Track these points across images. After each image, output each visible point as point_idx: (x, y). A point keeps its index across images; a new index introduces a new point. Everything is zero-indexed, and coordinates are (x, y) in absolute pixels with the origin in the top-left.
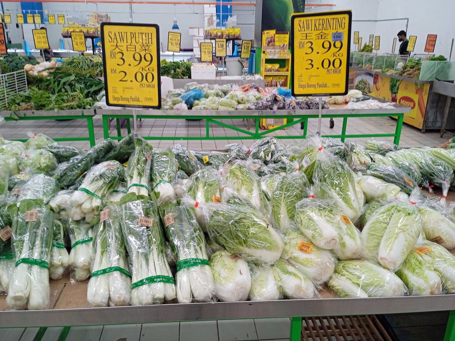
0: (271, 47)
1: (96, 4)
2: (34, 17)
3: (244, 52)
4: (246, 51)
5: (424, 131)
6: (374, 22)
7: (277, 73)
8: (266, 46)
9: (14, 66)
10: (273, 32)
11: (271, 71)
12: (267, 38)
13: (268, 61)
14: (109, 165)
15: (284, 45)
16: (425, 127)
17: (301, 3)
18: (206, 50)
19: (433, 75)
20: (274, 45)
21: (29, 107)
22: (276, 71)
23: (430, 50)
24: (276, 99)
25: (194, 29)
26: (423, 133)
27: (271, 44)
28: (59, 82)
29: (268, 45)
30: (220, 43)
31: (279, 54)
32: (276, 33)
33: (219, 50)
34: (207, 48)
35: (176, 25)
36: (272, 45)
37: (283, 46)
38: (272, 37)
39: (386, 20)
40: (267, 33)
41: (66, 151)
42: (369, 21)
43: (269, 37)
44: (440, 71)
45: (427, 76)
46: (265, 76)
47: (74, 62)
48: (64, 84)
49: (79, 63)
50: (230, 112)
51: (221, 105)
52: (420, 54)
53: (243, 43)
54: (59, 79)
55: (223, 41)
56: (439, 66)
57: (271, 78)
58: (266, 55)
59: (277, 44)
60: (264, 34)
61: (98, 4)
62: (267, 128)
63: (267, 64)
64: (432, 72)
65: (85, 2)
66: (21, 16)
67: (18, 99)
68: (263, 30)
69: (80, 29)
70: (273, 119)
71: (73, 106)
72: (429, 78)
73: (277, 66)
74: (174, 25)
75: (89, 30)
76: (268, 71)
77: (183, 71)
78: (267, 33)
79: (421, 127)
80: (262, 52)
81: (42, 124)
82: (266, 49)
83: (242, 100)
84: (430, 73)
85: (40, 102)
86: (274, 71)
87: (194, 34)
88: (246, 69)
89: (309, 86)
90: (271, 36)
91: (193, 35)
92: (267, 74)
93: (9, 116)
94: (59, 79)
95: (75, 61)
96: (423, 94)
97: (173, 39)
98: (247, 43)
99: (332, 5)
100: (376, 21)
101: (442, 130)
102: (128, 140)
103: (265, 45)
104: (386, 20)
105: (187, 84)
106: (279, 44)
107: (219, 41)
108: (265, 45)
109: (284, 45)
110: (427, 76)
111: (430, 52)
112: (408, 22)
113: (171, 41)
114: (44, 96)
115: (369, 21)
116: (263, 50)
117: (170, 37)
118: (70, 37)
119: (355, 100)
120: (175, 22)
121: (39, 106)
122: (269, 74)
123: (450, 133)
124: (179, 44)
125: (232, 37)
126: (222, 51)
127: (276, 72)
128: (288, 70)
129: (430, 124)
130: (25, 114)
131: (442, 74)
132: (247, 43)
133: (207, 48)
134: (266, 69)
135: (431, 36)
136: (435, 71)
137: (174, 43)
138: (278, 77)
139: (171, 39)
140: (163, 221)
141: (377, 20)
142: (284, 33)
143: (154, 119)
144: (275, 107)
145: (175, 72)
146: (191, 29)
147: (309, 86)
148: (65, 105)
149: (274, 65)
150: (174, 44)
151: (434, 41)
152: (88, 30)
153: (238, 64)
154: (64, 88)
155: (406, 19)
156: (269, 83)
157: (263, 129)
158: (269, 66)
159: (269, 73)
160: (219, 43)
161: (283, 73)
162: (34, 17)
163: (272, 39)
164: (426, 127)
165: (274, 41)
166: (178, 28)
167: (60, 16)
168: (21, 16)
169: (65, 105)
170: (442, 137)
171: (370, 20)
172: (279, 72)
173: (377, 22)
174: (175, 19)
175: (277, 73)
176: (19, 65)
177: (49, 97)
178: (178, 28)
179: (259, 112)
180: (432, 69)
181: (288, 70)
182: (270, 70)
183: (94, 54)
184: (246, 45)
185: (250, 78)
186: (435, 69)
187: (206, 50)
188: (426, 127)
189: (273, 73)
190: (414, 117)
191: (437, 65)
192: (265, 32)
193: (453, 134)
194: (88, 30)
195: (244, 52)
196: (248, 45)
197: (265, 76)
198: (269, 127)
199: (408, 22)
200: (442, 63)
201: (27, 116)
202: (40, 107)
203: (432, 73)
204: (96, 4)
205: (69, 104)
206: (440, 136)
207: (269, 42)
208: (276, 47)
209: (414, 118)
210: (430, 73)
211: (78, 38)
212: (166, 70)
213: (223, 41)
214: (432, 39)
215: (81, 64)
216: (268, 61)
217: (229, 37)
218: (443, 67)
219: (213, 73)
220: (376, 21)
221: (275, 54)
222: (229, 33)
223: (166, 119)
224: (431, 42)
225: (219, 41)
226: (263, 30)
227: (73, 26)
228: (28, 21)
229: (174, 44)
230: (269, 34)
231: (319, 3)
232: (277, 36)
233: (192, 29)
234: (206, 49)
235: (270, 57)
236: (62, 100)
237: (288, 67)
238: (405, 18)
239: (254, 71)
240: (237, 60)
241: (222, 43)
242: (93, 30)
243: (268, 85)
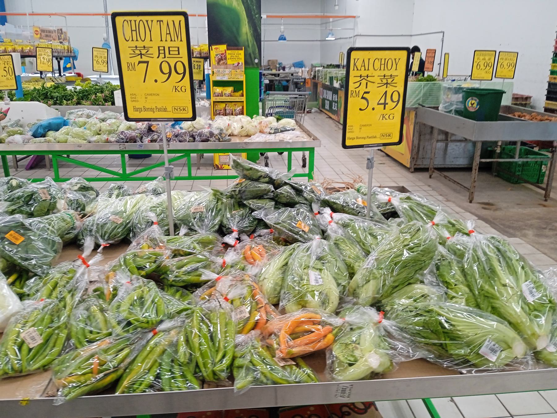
0: (222, 66)
1: (65, 17)
5: (413, 170)
6: (409, 37)
7: (229, 99)
8: (216, 65)
10: (223, 47)
12: (217, 55)
15: (239, 63)
16: (413, 165)
17: (256, 11)
19: (419, 99)
20: (226, 64)
24: (151, 129)
26: (412, 172)
27: (222, 62)
29: (218, 63)
31: (230, 75)
32: (228, 49)
36: (224, 63)
37: (238, 65)
38: (222, 54)
39: (421, 34)
40: (216, 49)
42: (402, 35)
43: (218, 53)
44: (428, 95)
45: (411, 102)
46: (214, 102)
52: (452, 76)
56: (426, 88)
57: (224, 105)
59: (229, 62)
60: (212, 50)
61: (67, 17)
64: (418, 94)
65: (27, 14)
69: (13, 47)
72: (413, 105)
73: (229, 90)
75: (24, 48)
76: (218, 96)
78: (216, 49)
79: (408, 166)
83: (100, 131)
84: (415, 98)
86: (226, 96)
89: (146, 110)
90: (221, 53)
92: (216, 99)
96: (410, 123)
97: (99, 55)
98: (197, 62)
99: (354, 17)
100: (411, 36)
101: (430, 169)
103: (214, 63)
104: (421, 34)
106: (232, 63)
109: (239, 63)
110: (411, 102)
111: (429, 71)
112: (443, 36)
113: (97, 59)
115: (402, 35)
117: (95, 53)
118: (35, 56)
119: (272, 131)
123: (438, 172)
124: (106, 62)
125: (205, 55)
127: (228, 98)
128: (243, 96)
129: (419, 162)
131: (430, 98)
132: (197, 62)
135: (430, 51)
136: (422, 94)
137: (100, 60)
138: (233, 103)
139: (96, 56)
141: (412, 34)
142: (238, 49)
144: (146, 140)
145: (96, 97)
147: (146, 110)
150: (100, 62)
151: (433, 57)
152: (22, 48)
155: (441, 32)
156: (221, 110)
158: (219, 90)
161: (237, 98)
164: (415, 165)
165: (226, 59)
170: (430, 177)
171: (404, 34)
172: (232, 98)
173: (413, 37)
175: (229, 99)
179: (121, 146)
180: (417, 93)
181: (243, 96)
182: (221, 95)
183: (41, 78)
186: (421, 92)
188: (415, 165)
190: (403, 153)
191: (423, 88)
192: (214, 47)
193: (440, 173)
194: (22, 48)
196: (199, 64)
198: (223, 166)
199: (443, 36)
200: (429, 85)
203: (418, 98)
204: (65, 17)
206: (428, 176)
207: (219, 60)
208: (229, 66)
209: (403, 154)
210: (415, 98)
212: (85, 95)
214: (430, 55)
217: (200, 54)
218: (431, 90)
220: (411, 36)
221: (224, 75)
222: (200, 50)
224: (430, 58)
226: (210, 45)
227: (22, 44)
229: (100, 62)
231: (344, 15)
232: (228, 52)
235: (218, 78)
237: (243, 91)
238: (440, 31)
242: (29, 48)
243: (220, 113)
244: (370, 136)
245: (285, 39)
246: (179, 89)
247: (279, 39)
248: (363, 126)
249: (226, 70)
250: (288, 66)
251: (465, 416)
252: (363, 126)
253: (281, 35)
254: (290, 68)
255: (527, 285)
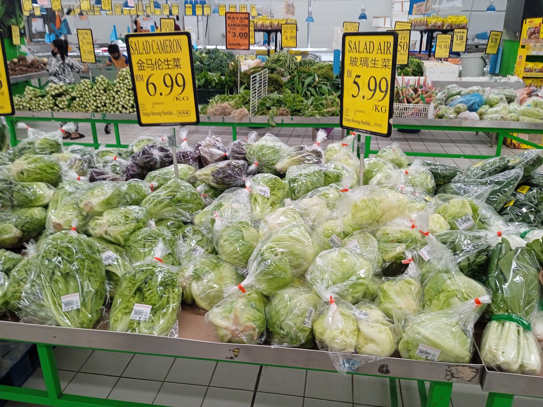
2: (203, 8)
3: (491, 47)
4: (493, 44)
9: (218, 64)
11: (531, 71)
12: (529, 29)
13: (530, 59)
14: (276, 178)
18: (443, 44)
20: (538, 38)
21: (285, 112)
22: (539, 72)
23: (239, 45)
25: (379, 19)
27: (534, 36)
28: (303, 83)
30: (459, 35)
33: (457, 44)
34: (445, 40)
35: (364, 14)
36: (536, 37)
38: (536, 28)
40: (530, 22)
41: (446, 170)
47: (280, 60)
48: (309, 85)
49: (286, 61)
50: (536, 125)
51: (523, 115)
53: (491, 35)
54: (303, 80)
55: (463, 32)
58: (528, 50)
60: (526, 23)
62: (518, 146)
63: (528, 63)
66: (190, 7)
67: (269, 102)
68: (525, 17)
70: (527, 135)
71: (335, 112)
74: (362, 14)
76: (528, 72)
77: (414, 70)
78: (530, 22)
80: (520, 46)
81: (223, 131)
82: (526, 42)
85: (294, 106)
87: (379, 25)
88: (487, 69)
89: (353, 121)
91: (377, 26)
93: (267, 122)
94: (303, 80)
95: (281, 58)
98: (495, 35)
102: (535, 159)
105: (448, 87)
107: (458, 32)
108: (525, 37)
114: (297, 100)
116: (521, 44)
120: (363, 10)
121: (293, 111)
122: (529, 76)
126: (460, 44)
127: (540, 74)
130: (282, 121)
132: (495, 35)
133: (445, 40)
134: (525, 68)
138: (539, 80)
140: (490, 262)
143: (305, 129)
146: (375, 19)
147: (353, 121)
148: (325, 110)
149: (537, 63)
153: (481, 61)
154: (308, 90)
157: (512, 147)
158: (530, 65)
159: (529, 75)
160: (458, 34)
162: (203, 8)
163: (537, 29)
165: (539, 33)
166: (366, 18)
167: (232, 7)
168: (190, 7)
169: (325, 110)
174: (363, 7)
176: (223, 63)
177: (302, 102)
178: (366, 18)
182: (530, 70)
184: (494, 37)
185: (502, 81)
187: (443, 44)
189: (534, 74)
192: (528, 20)
195: (491, 47)
196: (496, 37)
197: (523, 78)
198: (521, 145)
201: (284, 122)
202: (296, 112)
205: (328, 109)
207: (532, 34)
211: (289, 31)
213: (463, 32)
215: (288, 62)
216: (530, 59)
217: (451, 27)
219: (455, 72)
223: (293, 128)
225: (458, 32)
228: (197, 13)
230: (532, 24)
233: (377, 19)
234: (443, 42)
235: (534, 53)
236: (322, 104)
239: (497, 71)
240: (480, 56)
241: (462, 34)
244: (364, 121)
245: (494, 10)
246: (181, 99)
247: (488, 10)
248: (358, 111)
249: (537, 44)
250: (471, 38)
251: (404, 405)
252: (358, 111)
253: (491, 6)
254: (473, 39)
255: (460, 224)
